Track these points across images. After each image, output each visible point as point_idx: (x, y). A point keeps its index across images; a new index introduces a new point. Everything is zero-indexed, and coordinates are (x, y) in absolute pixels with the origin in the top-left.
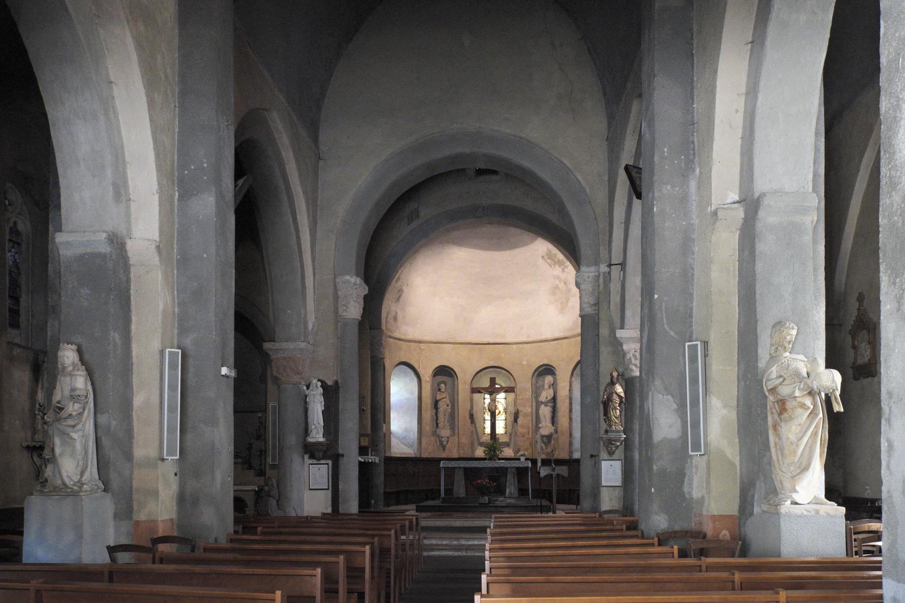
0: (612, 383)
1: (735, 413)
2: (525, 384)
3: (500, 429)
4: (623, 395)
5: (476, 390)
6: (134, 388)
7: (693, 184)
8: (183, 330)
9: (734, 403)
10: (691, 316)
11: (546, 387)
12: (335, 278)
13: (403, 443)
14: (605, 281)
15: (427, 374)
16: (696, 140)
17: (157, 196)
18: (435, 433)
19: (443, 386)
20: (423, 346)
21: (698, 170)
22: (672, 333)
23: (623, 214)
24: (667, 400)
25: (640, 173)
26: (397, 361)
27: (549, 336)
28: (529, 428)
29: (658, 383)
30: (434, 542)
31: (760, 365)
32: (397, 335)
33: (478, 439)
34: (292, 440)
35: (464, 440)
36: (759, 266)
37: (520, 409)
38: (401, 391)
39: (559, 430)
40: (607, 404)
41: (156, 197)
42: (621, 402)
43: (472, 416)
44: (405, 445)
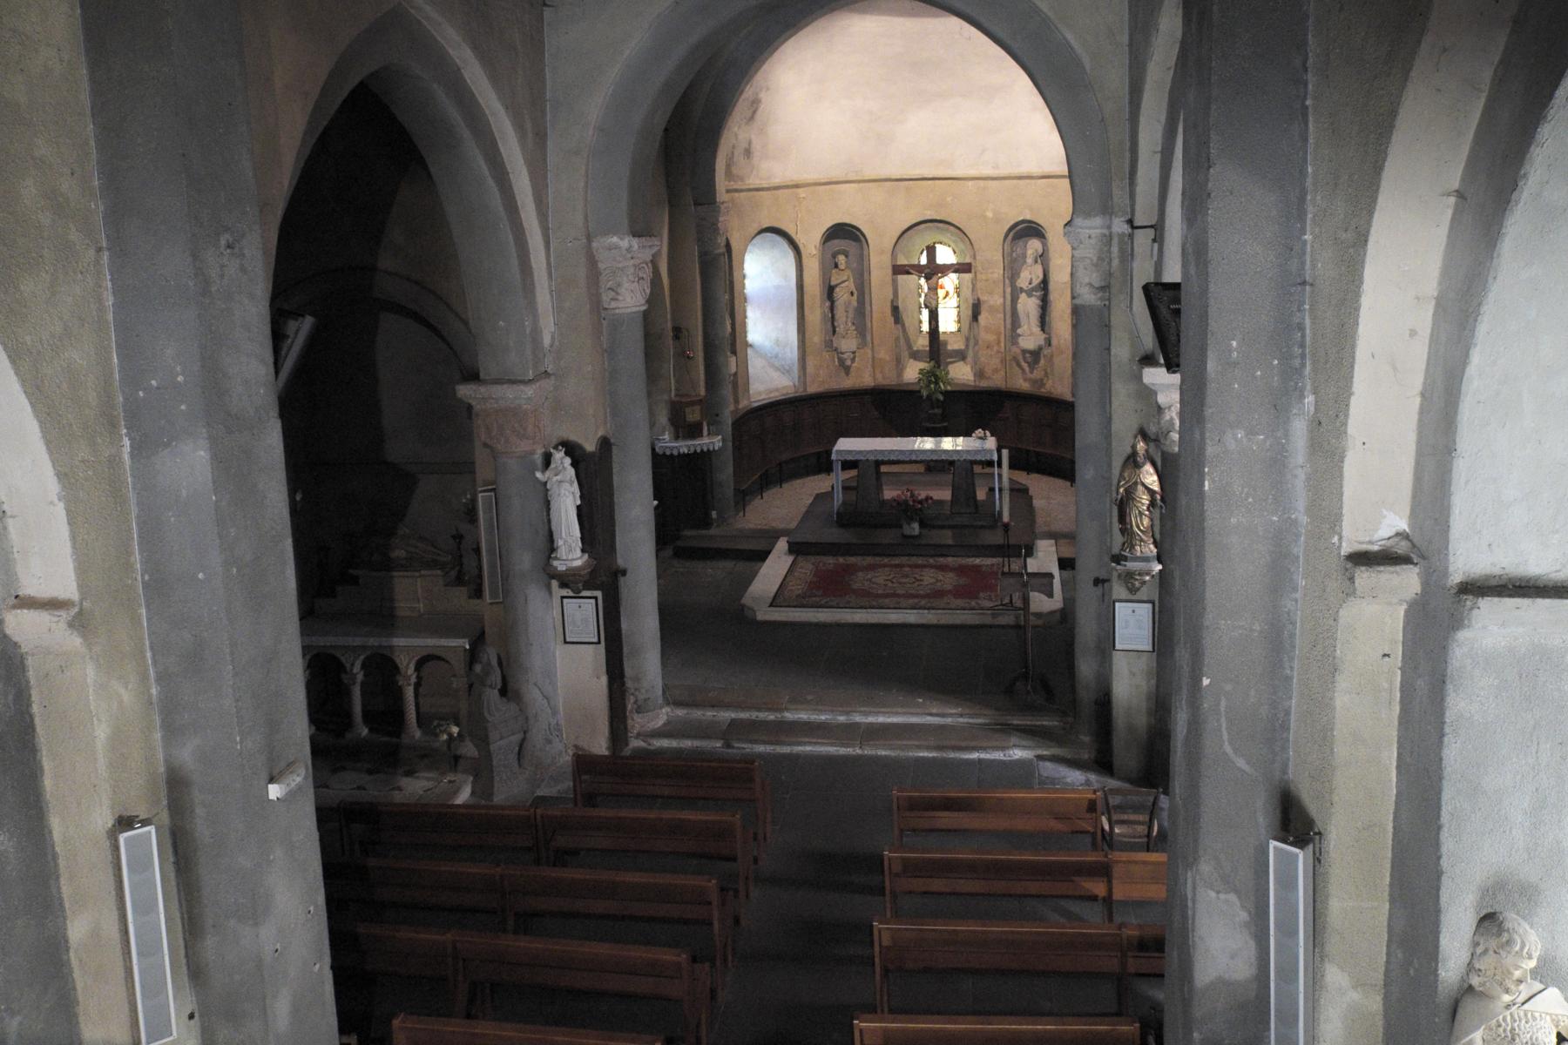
0: (1132, 461)
1: (1379, 998)
2: (991, 255)
3: (948, 322)
4: (1156, 487)
5: (899, 270)
6: (67, 906)
7: (1299, 429)
8: (172, 731)
9: (1379, 976)
10: (1285, 727)
11: (1029, 260)
12: (589, 238)
13: (772, 366)
14: (1122, 251)
15: (811, 241)
16: (1308, 322)
17: (61, 505)
18: (829, 344)
19: (841, 259)
20: (802, 192)
21: (1310, 399)
22: (1241, 763)
23: (1156, 174)
24: (1227, 901)
25: (1177, 300)
26: (756, 227)
27: (1036, 171)
28: (999, 334)
29: (1205, 867)
30: (803, 716)
31: (1442, 973)
32: (753, 181)
33: (909, 346)
34: (524, 560)
35: (884, 354)
36: (1453, 753)
37: (982, 298)
38: (763, 274)
39: (1054, 342)
40: (1124, 506)
41: (60, 509)
42: (1152, 504)
43: (895, 310)
44: (777, 369)
